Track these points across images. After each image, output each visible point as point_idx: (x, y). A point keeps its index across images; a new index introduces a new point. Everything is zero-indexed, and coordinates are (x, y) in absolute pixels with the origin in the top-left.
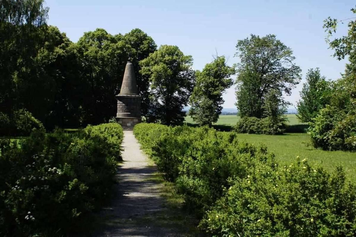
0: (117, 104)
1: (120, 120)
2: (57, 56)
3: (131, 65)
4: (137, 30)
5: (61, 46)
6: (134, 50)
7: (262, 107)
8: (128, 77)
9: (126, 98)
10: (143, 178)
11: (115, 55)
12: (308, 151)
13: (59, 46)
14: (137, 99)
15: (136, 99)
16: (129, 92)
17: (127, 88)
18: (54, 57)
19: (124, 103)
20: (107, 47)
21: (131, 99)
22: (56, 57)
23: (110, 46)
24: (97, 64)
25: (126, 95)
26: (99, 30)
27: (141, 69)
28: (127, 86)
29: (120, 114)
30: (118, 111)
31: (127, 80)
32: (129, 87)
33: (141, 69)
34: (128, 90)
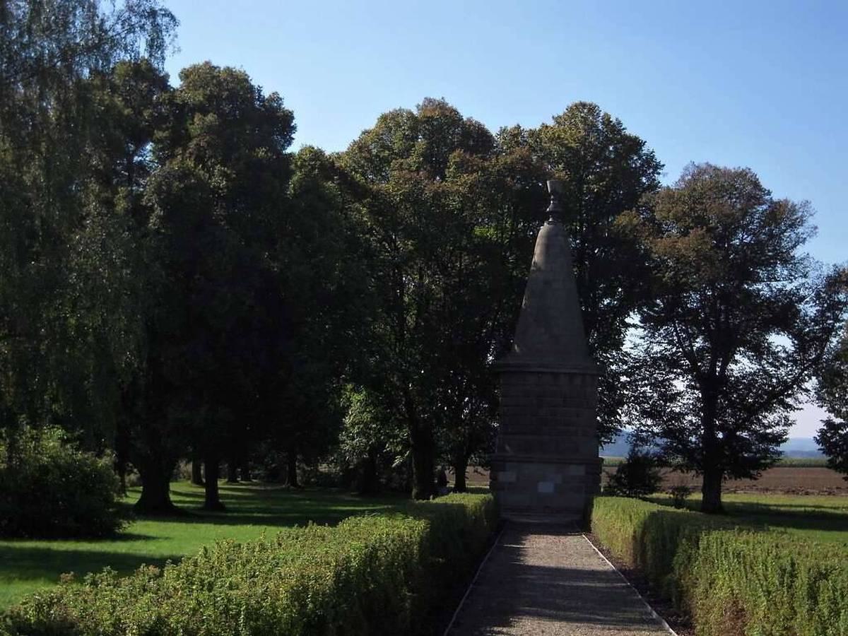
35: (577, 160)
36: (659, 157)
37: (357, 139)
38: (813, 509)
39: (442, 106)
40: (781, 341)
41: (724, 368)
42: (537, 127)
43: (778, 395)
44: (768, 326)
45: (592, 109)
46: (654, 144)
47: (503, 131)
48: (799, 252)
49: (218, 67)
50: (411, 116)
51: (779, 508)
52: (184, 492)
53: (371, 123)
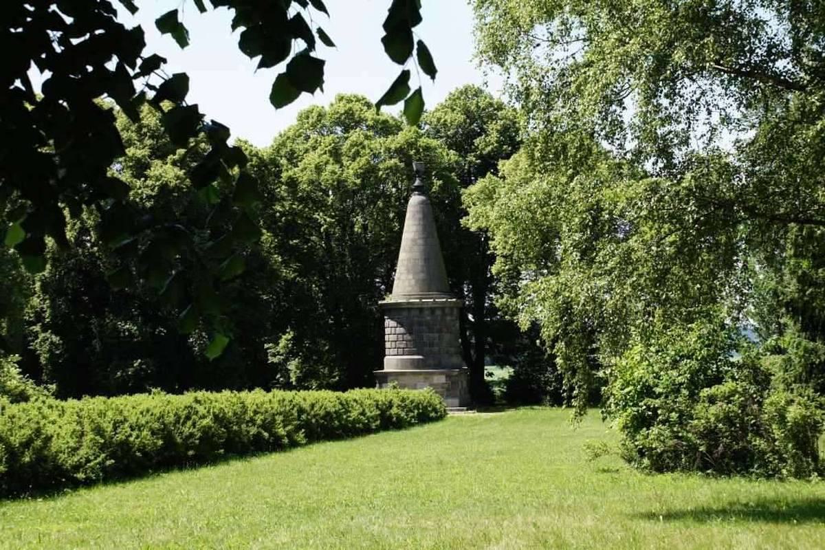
0: (383, 329)
1: (389, 379)
2: (156, 188)
3: (423, 203)
4: (465, 92)
5: (176, 157)
6: (453, 155)
7: (22, 376)
8: (414, 240)
9: (404, 309)
10: (702, 515)
11: (381, 173)
12: (660, 526)
13: (170, 158)
14: (443, 309)
15: (438, 313)
16: (416, 288)
17: (411, 277)
18: (150, 192)
19: (402, 326)
20: (353, 150)
21: (421, 310)
22: (153, 194)
23: (364, 147)
24: (320, 205)
25: (405, 301)
26: (341, 99)
27: (467, 214)
28: (408, 272)
29: (391, 363)
30: (387, 352)
31: (411, 250)
32: (415, 274)
33: (467, 214)
34: (413, 282)
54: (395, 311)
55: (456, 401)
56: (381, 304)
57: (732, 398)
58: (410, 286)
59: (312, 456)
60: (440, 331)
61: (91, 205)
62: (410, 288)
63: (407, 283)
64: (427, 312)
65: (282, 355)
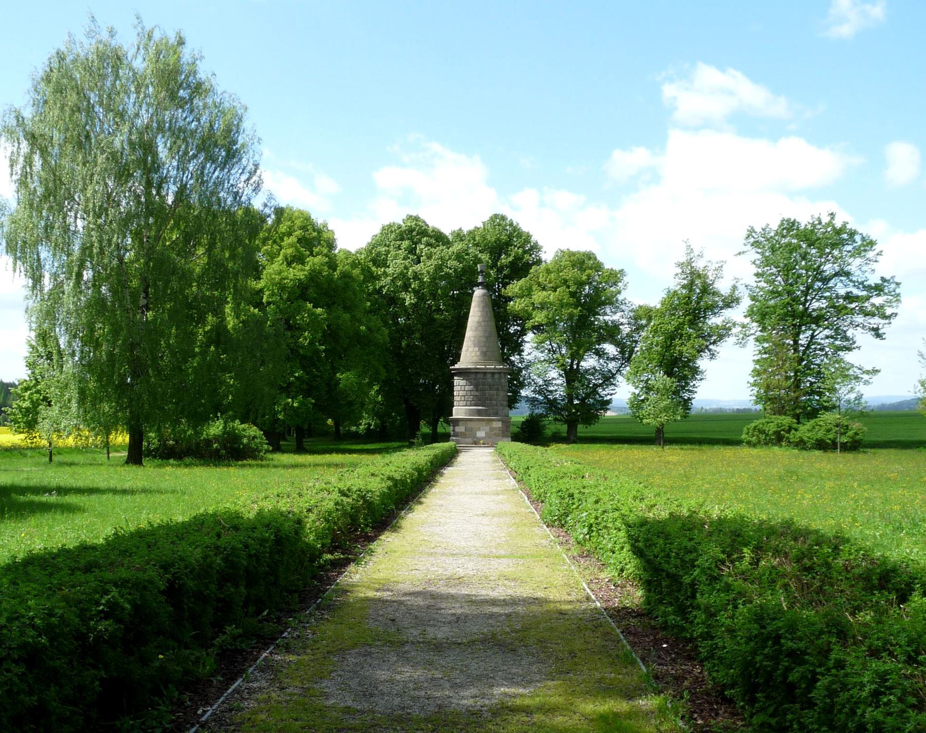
1: (460, 423)
3: (484, 295)
17: (477, 349)
32: (479, 347)
34: (478, 353)
35: (498, 248)
36: (540, 243)
37: (370, 241)
38: (342, 447)
39: (417, 219)
40: (610, 349)
41: (578, 365)
42: (472, 228)
43: (608, 379)
44: (601, 340)
45: (503, 218)
46: (537, 237)
47: (453, 233)
48: (620, 297)
49: (782, 221)
50: (399, 227)
51: (401, 444)
52: (717, 448)
53: (377, 230)
54: (463, 373)
55: (510, 439)
56: (405, 442)
57: (616, 613)
58: (476, 356)
59: (130, 483)
60: (498, 390)
61: (756, 698)
62: (476, 358)
63: (473, 354)
64: (489, 376)
65: (234, 134)
